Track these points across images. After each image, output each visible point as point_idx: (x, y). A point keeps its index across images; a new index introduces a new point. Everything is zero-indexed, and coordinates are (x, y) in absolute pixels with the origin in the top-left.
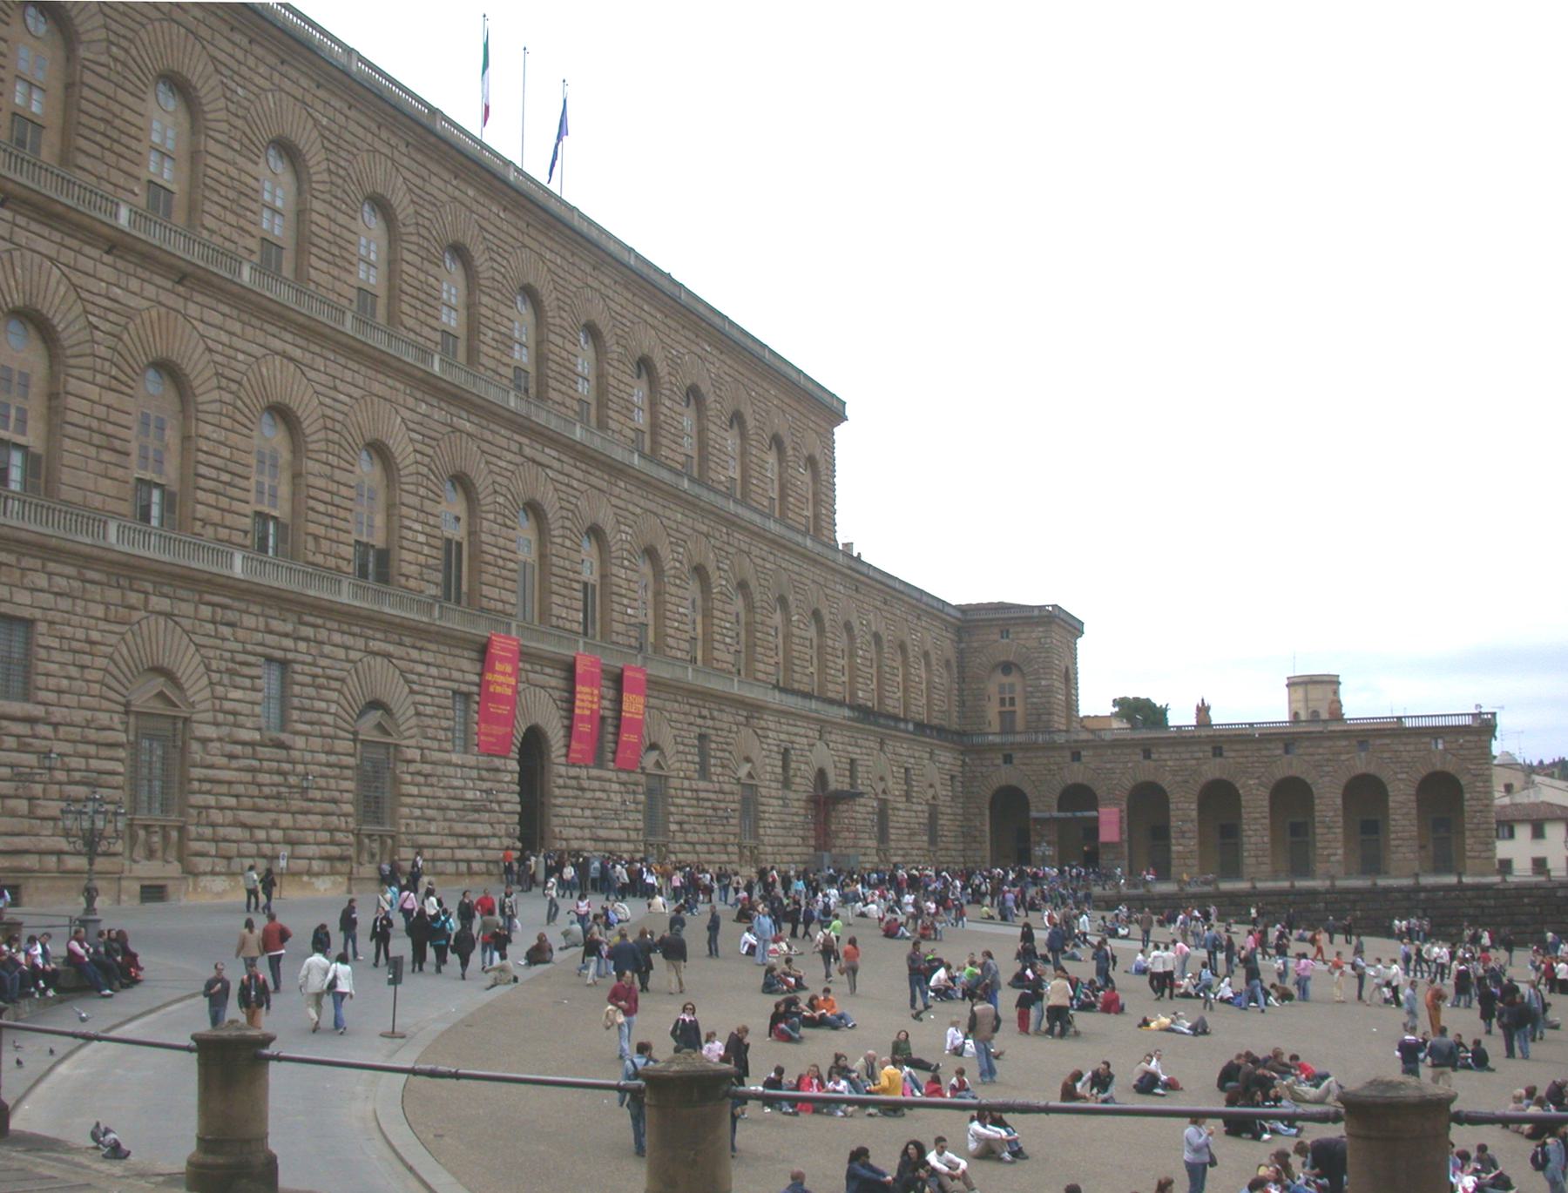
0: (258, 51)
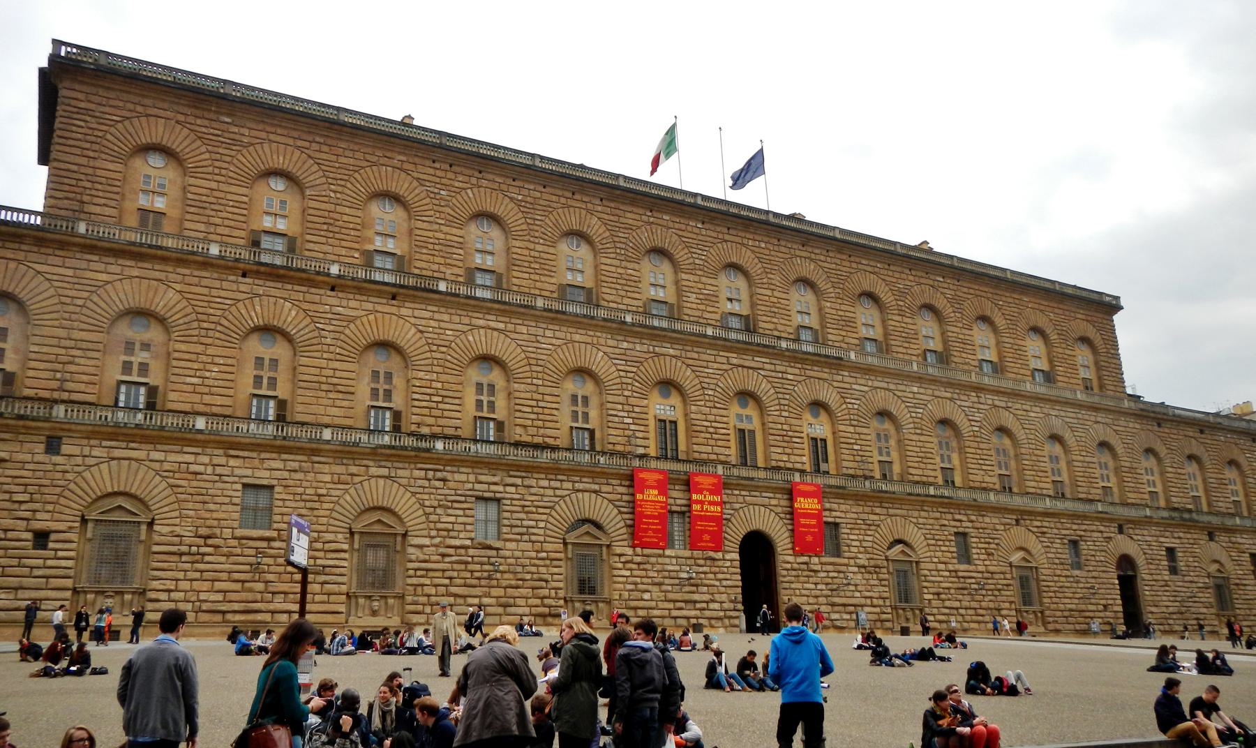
0: (783, 243)
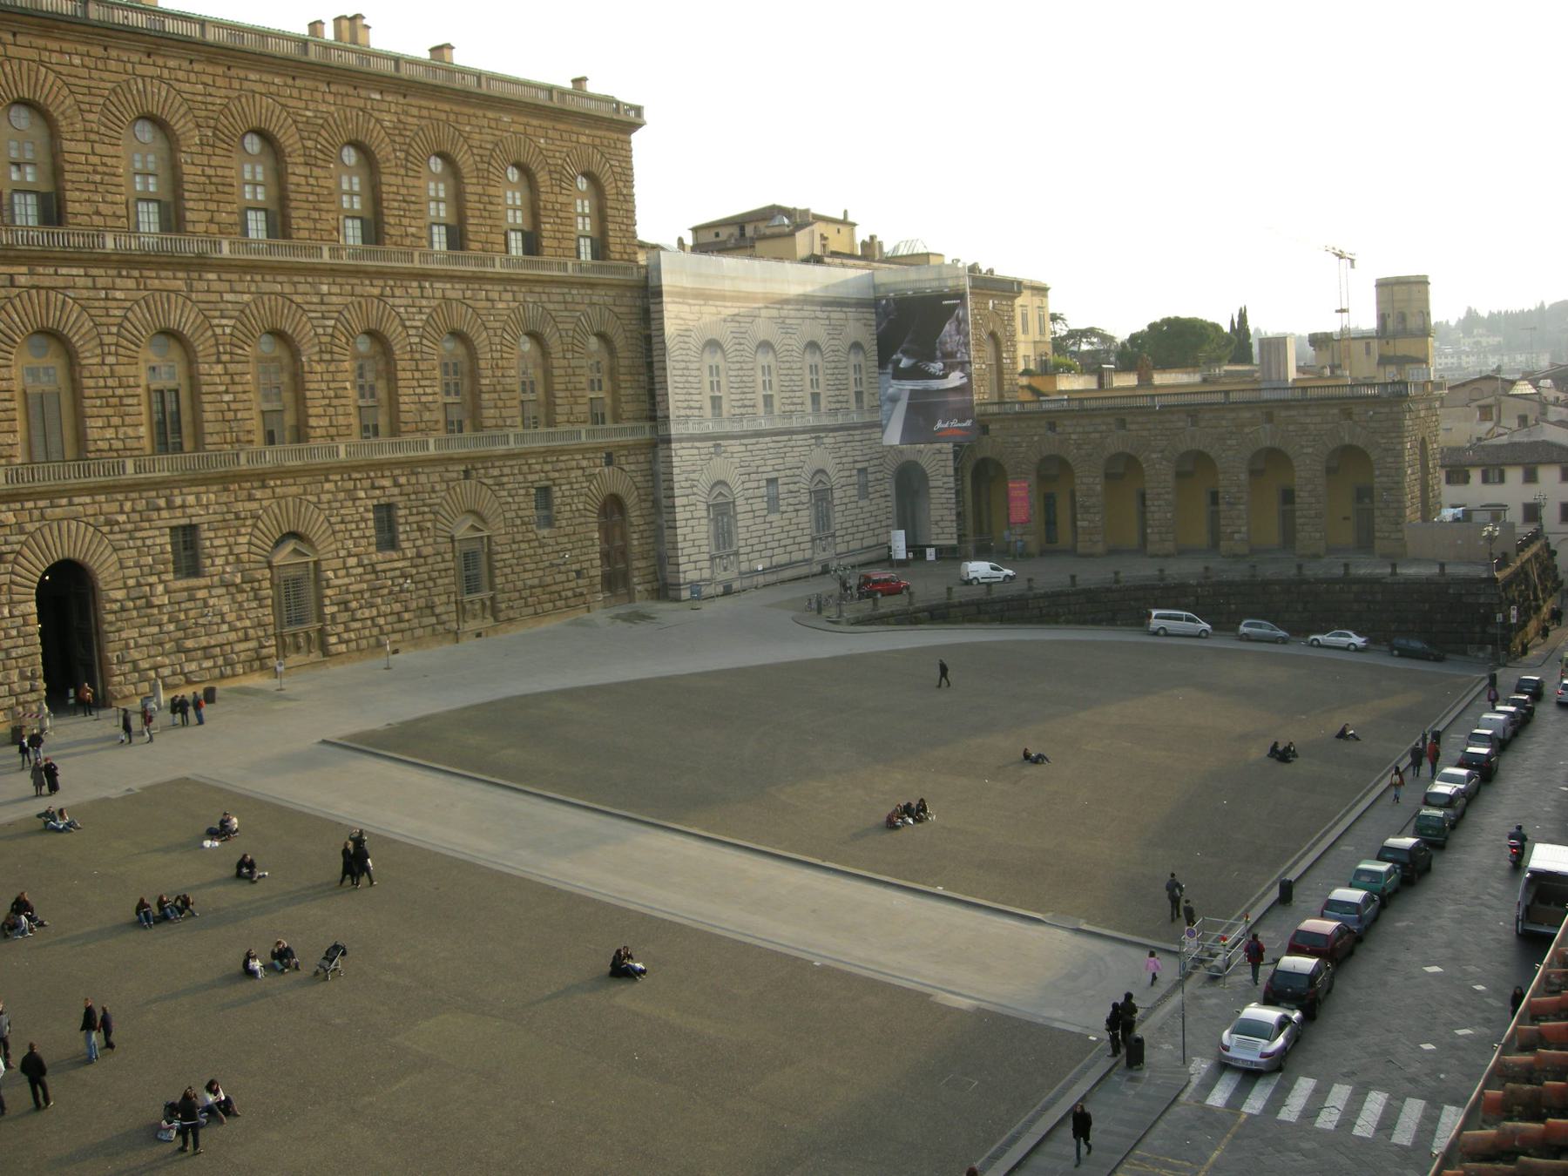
0: (114, 53)
